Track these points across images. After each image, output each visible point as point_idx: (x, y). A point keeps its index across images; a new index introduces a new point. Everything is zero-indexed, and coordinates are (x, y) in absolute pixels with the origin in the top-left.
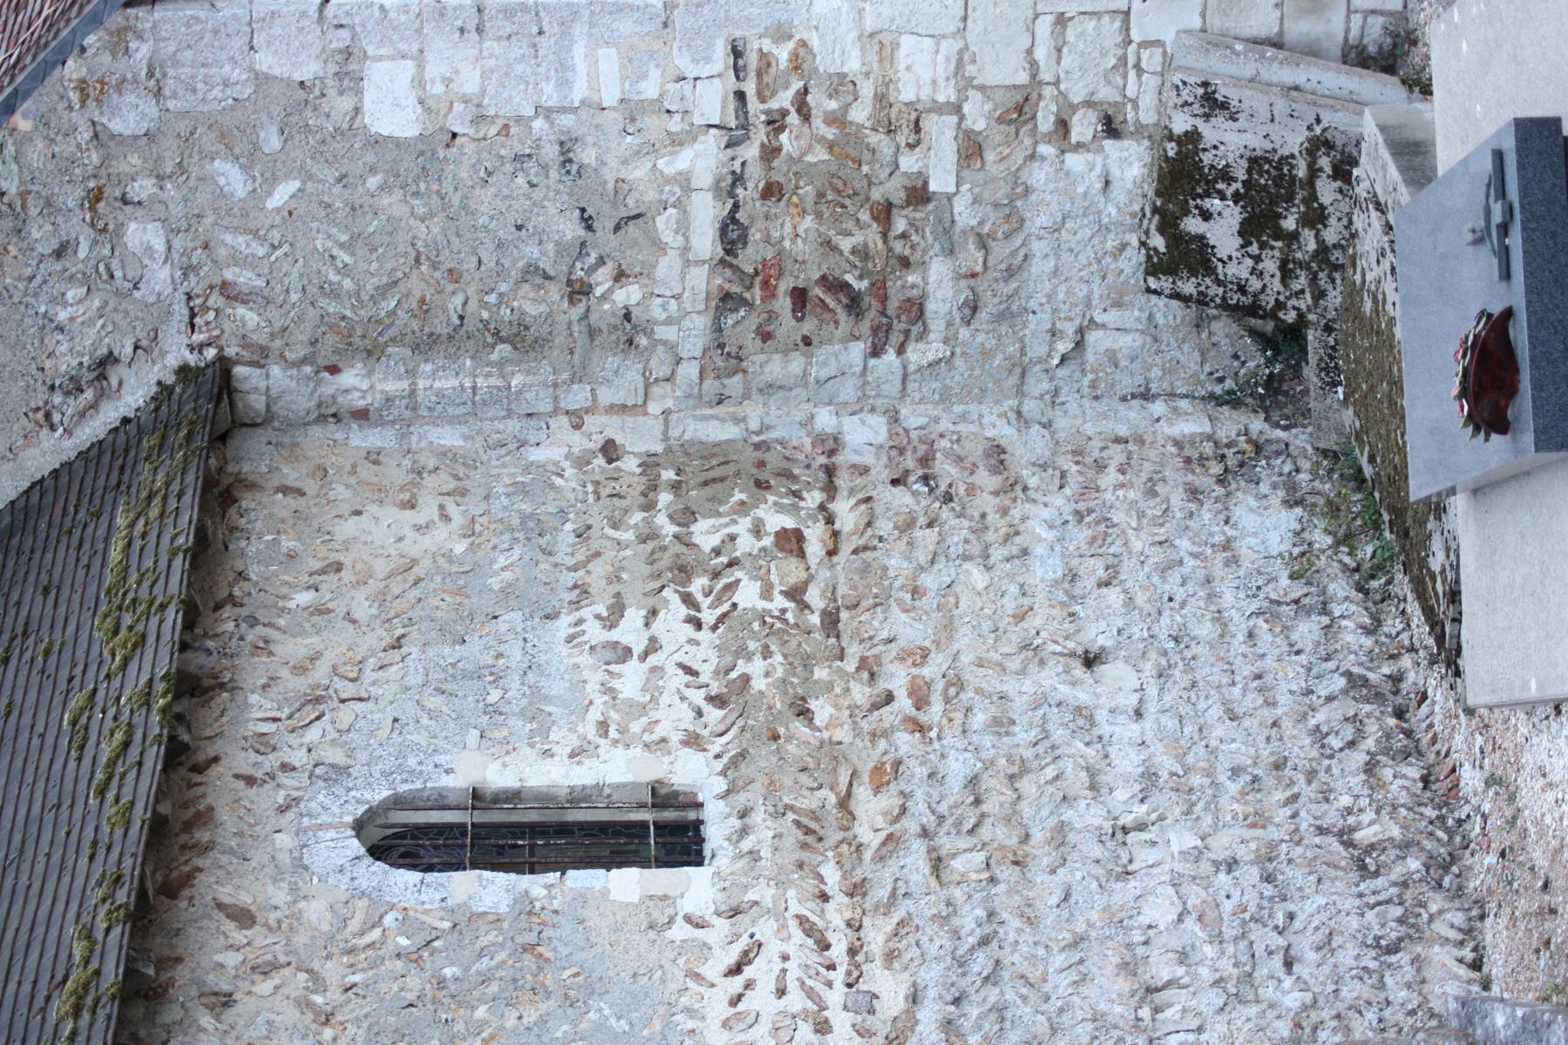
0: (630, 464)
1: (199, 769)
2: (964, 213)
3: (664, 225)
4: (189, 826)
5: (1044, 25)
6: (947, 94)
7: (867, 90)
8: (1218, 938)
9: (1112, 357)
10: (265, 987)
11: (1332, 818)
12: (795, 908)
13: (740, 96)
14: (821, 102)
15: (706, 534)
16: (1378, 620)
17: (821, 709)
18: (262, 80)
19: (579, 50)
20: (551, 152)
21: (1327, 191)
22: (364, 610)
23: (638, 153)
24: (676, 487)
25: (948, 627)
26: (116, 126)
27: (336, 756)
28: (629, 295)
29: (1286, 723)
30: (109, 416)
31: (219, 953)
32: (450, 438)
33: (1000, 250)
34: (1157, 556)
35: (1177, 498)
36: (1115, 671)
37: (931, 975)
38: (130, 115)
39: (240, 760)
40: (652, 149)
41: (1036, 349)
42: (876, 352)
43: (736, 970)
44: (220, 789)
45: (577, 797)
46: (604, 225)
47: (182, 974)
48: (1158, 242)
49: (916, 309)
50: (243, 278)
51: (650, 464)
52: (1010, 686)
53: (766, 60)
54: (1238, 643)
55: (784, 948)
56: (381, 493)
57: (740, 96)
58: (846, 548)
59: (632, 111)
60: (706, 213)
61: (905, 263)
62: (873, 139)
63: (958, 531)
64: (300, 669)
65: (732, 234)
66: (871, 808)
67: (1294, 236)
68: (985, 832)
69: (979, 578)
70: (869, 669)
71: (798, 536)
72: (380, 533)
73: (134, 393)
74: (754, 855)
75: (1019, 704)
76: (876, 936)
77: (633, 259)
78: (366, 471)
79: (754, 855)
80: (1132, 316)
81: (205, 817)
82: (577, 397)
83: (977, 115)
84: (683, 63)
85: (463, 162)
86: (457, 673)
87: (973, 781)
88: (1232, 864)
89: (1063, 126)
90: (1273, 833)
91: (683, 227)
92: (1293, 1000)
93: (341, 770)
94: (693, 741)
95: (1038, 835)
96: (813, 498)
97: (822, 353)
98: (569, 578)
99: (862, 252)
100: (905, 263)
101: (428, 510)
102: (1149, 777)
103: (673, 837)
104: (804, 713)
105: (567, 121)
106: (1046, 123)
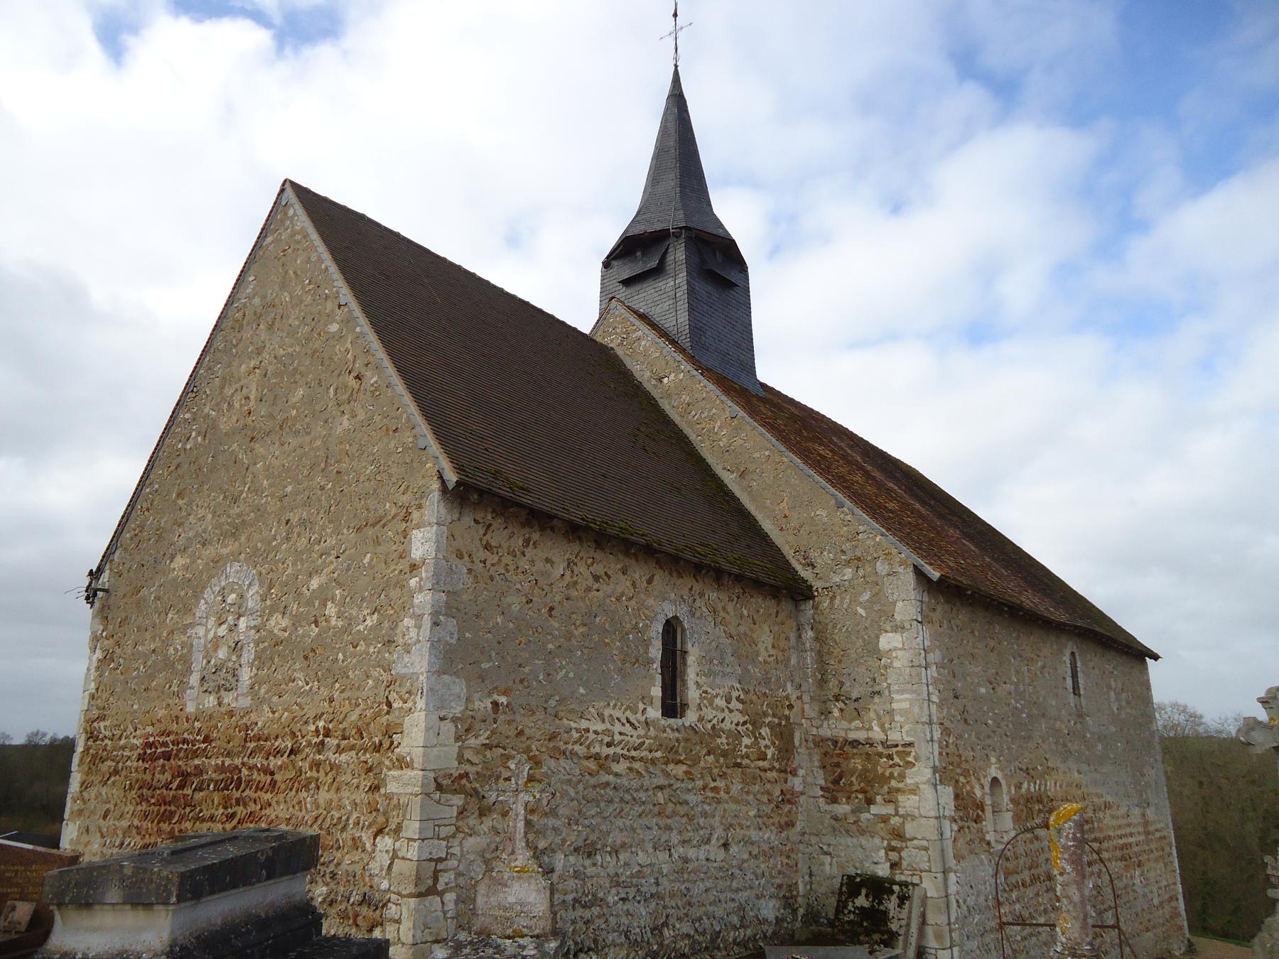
0: (787, 712)
1: (694, 576)
2: (864, 816)
3: (857, 723)
4: (677, 570)
5: (925, 843)
6: (901, 811)
7: (901, 785)
8: (632, 876)
9: (823, 864)
10: (628, 584)
11: (671, 921)
12: (647, 742)
13: (897, 746)
14: (896, 771)
15: (765, 731)
16: (738, 944)
17: (711, 758)
18: (894, 603)
19: (908, 696)
20: (877, 688)
21: (876, 937)
22: (742, 629)
23: (878, 715)
24: (780, 724)
25: (737, 802)
26: (878, 564)
27: (698, 614)
28: (836, 713)
29: (703, 909)
30: (798, 568)
31: (639, 573)
32: (793, 661)
33: (854, 828)
34: (759, 872)
35: (778, 881)
36: (721, 854)
37: (624, 781)
38: (882, 567)
39: (697, 587)
40: (879, 718)
41: (824, 839)
42: (822, 788)
43: (628, 721)
44: (688, 581)
45: (684, 683)
46: (856, 705)
47: (633, 562)
48: (858, 879)
49: (834, 801)
50: (837, 601)
51: (787, 718)
52: (717, 818)
53: (909, 754)
54: (730, 895)
55: (634, 736)
56: (776, 638)
57: (897, 746)
58: (762, 774)
59: (891, 713)
60: (861, 736)
61: (849, 798)
62: (886, 788)
63: (767, 809)
64: (724, 608)
65: (855, 743)
66: (681, 770)
67: (862, 925)
68: (670, 805)
69: (752, 813)
70: (723, 776)
71: (764, 759)
72: (765, 638)
73: (805, 573)
74: (664, 731)
75: (712, 821)
76: (637, 765)
77: (846, 714)
78: (783, 636)
79: (664, 731)
80: (835, 871)
81: (680, 576)
82: (806, 698)
83: (895, 821)
84: (906, 728)
85: (872, 662)
86: (722, 653)
87: (687, 803)
88: (657, 884)
89: (893, 849)
90: (667, 900)
91: (857, 729)
92: (610, 899)
93: (693, 615)
94: (701, 719)
95: (669, 821)
96: (776, 765)
97: (821, 772)
98: (752, 689)
99: (851, 784)
100: (849, 798)
101: (772, 652)
102: (686, 860)
103: (672, 707)
104: (709, 753)
105: (887, 693)
106: (894, 843)
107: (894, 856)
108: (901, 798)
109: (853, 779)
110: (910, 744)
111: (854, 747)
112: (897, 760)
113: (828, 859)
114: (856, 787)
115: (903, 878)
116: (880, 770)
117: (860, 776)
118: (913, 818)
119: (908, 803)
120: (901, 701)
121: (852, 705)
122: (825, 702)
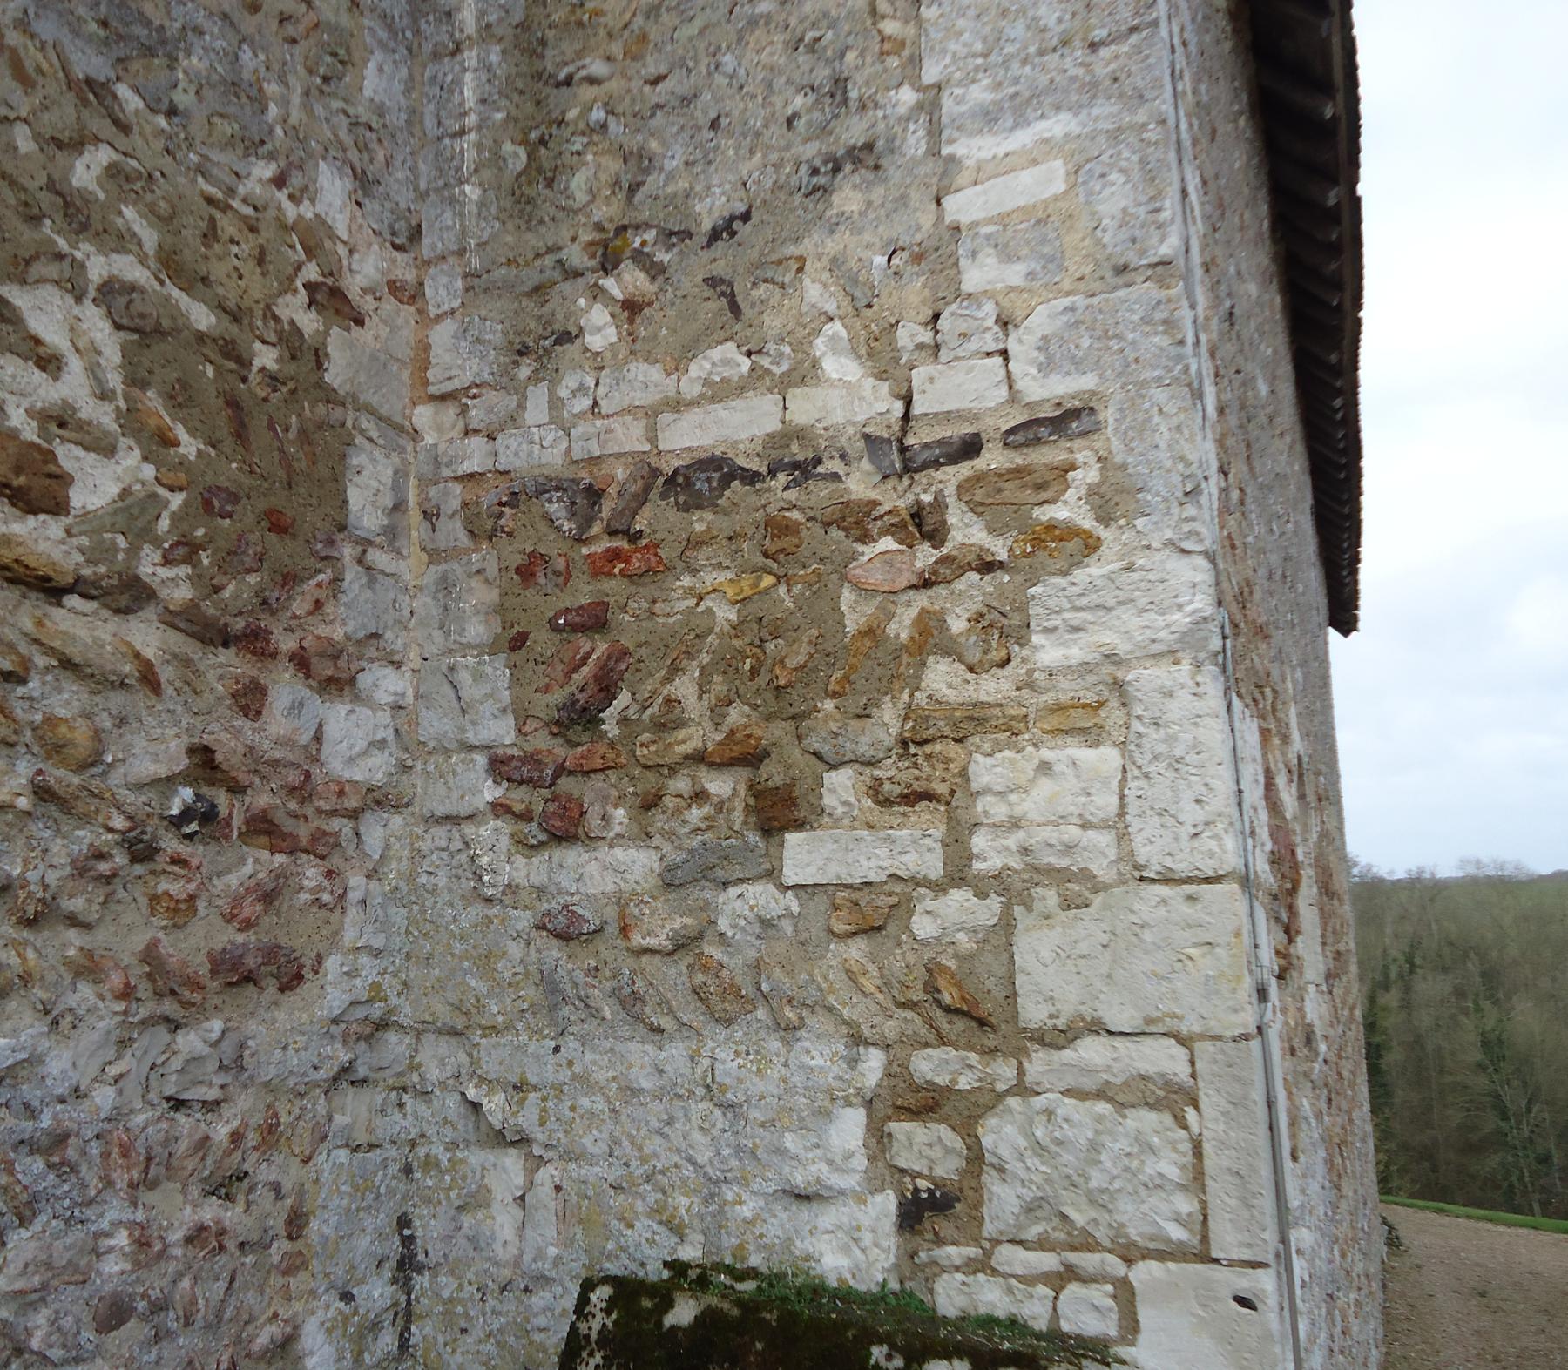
2: (741, 904)
5: (1165, 1059)
6: (991, 852)
7: (992, 687)
9: (477, 1201)
19: (1058, 125)
20: (854, 131)
28: (600, 328)
33: (674, 976)
41: (495, 1056)
42: (499, 767)
46: (721, 260)
48: (683, 1313)
49: (565, 828)
57: (971, 447)
60: (742, 427)
82: (442, 290)
83: (947, 918)
84: (1041, 320)
89: (927, 1103)
91: (719, 392)
97: (498, 670)
105: (915, 142)
106: (929, 1065)
107: (927, 1149)
108: (988, 769)
109: (684, 688)
110: (1067, 420)
111: (695, 503)
112: (967, 531)
113: (512, 1161)
114: (696, 736)
115: (991, 1298)
116: (854, 612)
117: (726, 663)
118: (1077, 889)
119: (1036, 795)
120: (1005, 166)
121: (692, 268)
122: (539, 291)
